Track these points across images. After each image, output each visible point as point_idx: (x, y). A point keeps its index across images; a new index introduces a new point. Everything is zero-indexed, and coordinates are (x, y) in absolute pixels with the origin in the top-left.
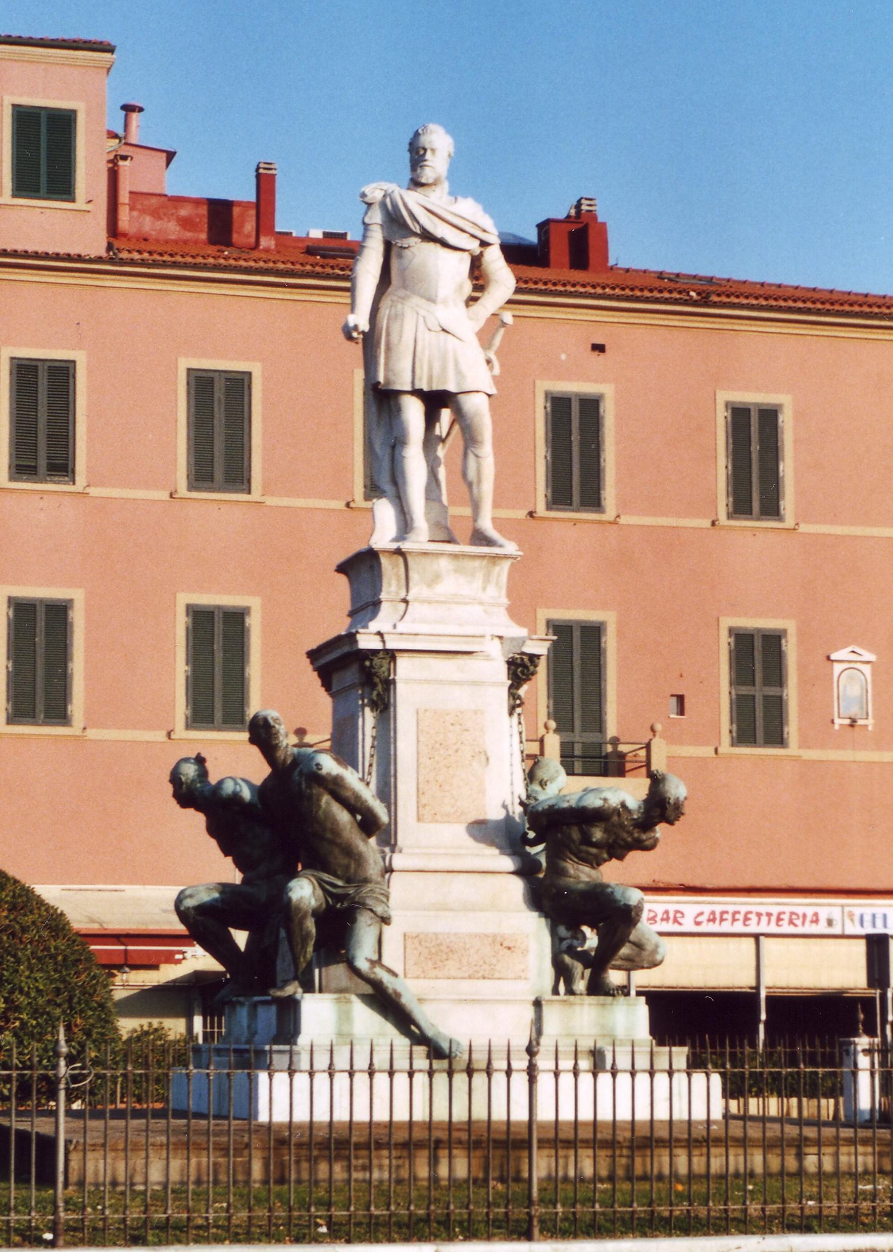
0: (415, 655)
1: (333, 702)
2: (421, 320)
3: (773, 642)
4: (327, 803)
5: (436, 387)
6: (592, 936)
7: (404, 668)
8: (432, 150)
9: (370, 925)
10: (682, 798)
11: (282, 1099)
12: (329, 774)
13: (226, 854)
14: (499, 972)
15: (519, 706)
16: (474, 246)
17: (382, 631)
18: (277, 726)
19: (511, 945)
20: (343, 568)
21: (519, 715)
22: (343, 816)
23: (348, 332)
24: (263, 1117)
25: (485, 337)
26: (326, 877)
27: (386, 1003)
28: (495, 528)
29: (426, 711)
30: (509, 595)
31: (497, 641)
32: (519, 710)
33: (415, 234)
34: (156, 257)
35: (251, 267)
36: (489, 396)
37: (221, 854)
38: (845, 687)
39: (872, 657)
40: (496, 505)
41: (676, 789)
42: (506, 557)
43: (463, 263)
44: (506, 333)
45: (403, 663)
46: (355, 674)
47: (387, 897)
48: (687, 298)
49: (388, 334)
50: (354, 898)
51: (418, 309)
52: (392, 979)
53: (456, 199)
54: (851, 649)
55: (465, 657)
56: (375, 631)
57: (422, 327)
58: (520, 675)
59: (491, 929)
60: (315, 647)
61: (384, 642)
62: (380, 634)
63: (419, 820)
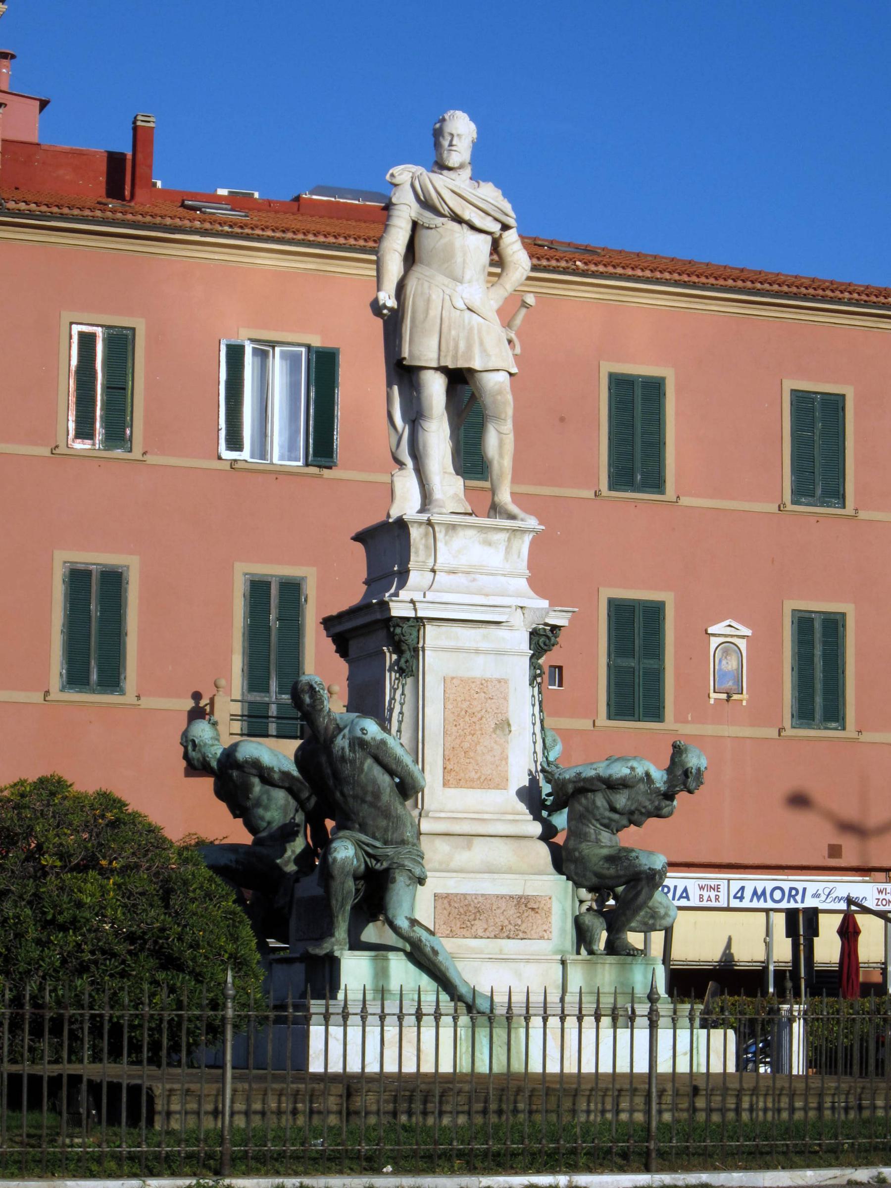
0: (480, 625)
1: (350, 667)
2: (447, 298)
3: (653, 613)
4: (370, 769)
5: (461, 364)
6: (617, 899)
7: (432, 636)
8: (458, 135)
9: (408, 886)
10: (702, 769)
11: (334, 1048)
12: (374, 739)
13: (236, 816)
14: (524, 932)
15: (540, 675)
16: (495, 228)
17: (415, 599)
18: (321, 691)
19: (535, 907)
20: (359, 538)
21: (539, 684)
22: (384, 780)
23: (377, 308)
24: (316, 1066)
25: (506, 317)
26: (364, 838)
27: (423, 959)
28: (514, 501)
29: (453, 678)
30: (529, 568)
31: (519, 610)
32: (539, 680)
33: (444, 216)
34: (44, 208)
35: (139, 222)
36: (511, 374)
37: (230, 816)
38: (720, 661)
39: (747, 632)
40: (515, 480)
41: (695, 760)
42: (523, 531)
43: (485, 243)
44: (526, 317)
45: (430, 630)
46: (377, 638)
47: (423, 858)
48: (574, 267)
49: (413, 312)
50: (393, 858)
51: (444, 288)
52: (431, 938)
53: (478, 183)
54: (727, 622)
55: (493, 627)
56: (409, 599)
57: (447, 303)
58: (542, 645)
59: (517, 891)
60: (335, 613)
61: (415, 610)
62: (412, 602)
63: (444, 785)
